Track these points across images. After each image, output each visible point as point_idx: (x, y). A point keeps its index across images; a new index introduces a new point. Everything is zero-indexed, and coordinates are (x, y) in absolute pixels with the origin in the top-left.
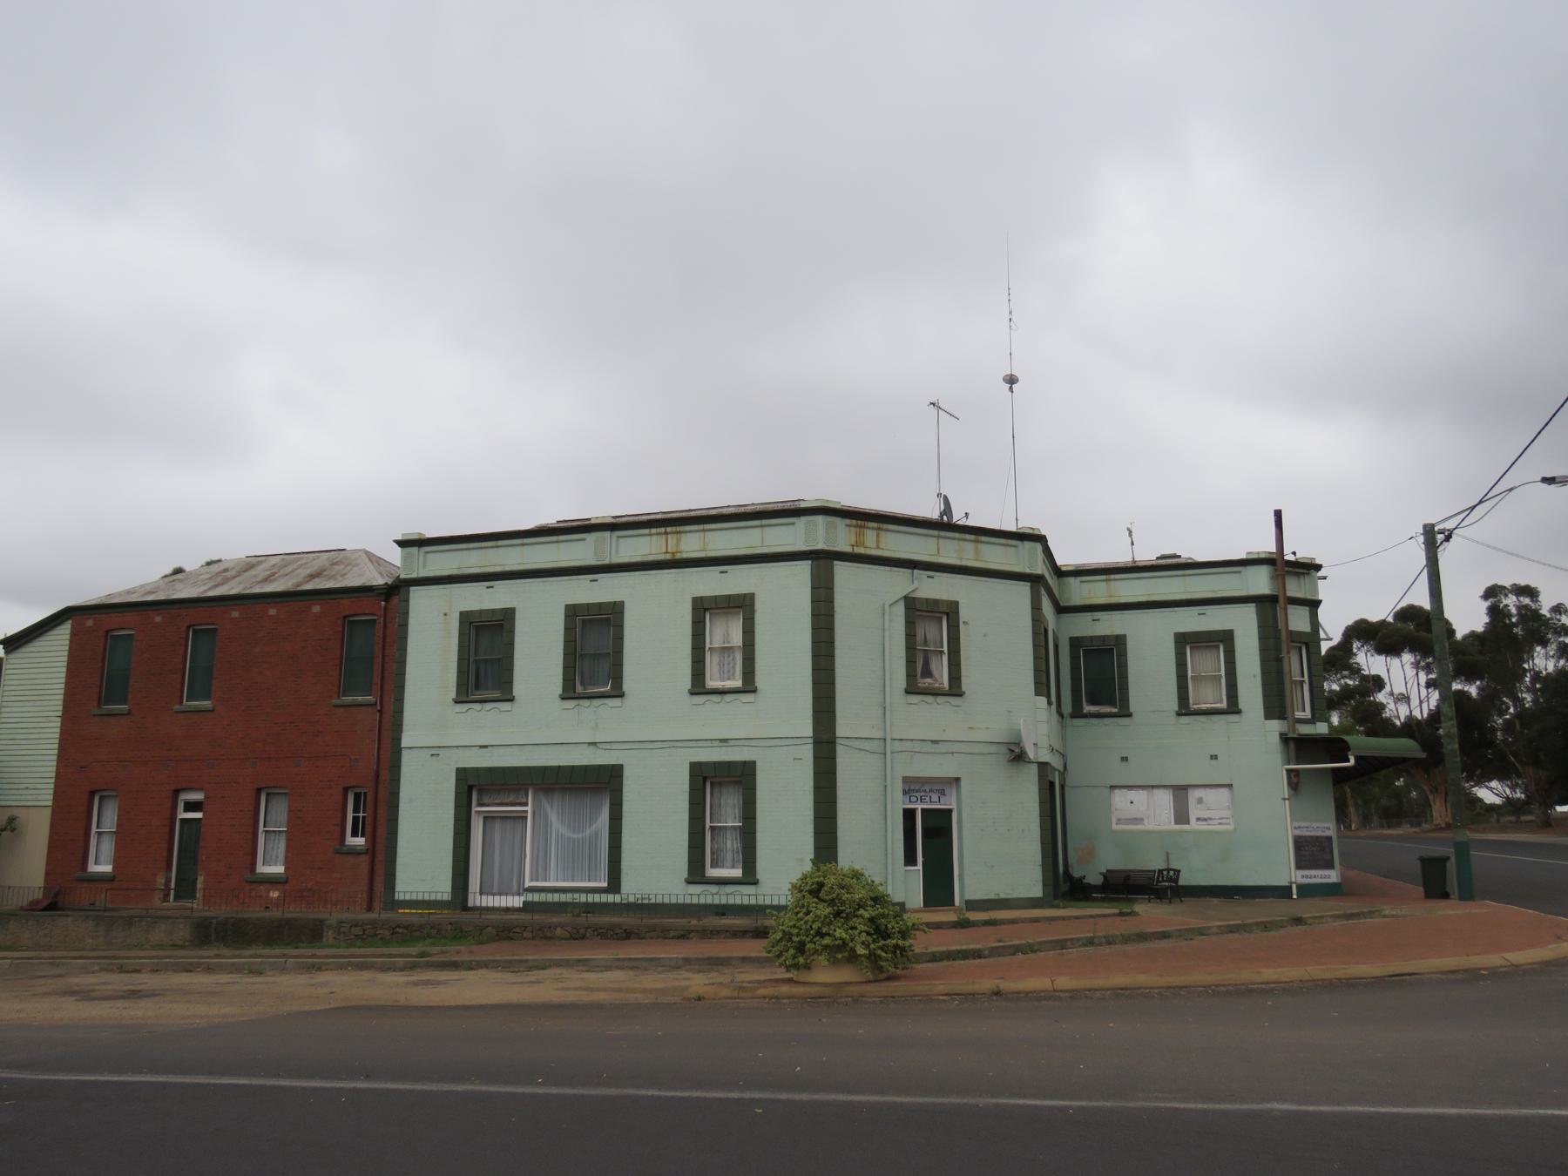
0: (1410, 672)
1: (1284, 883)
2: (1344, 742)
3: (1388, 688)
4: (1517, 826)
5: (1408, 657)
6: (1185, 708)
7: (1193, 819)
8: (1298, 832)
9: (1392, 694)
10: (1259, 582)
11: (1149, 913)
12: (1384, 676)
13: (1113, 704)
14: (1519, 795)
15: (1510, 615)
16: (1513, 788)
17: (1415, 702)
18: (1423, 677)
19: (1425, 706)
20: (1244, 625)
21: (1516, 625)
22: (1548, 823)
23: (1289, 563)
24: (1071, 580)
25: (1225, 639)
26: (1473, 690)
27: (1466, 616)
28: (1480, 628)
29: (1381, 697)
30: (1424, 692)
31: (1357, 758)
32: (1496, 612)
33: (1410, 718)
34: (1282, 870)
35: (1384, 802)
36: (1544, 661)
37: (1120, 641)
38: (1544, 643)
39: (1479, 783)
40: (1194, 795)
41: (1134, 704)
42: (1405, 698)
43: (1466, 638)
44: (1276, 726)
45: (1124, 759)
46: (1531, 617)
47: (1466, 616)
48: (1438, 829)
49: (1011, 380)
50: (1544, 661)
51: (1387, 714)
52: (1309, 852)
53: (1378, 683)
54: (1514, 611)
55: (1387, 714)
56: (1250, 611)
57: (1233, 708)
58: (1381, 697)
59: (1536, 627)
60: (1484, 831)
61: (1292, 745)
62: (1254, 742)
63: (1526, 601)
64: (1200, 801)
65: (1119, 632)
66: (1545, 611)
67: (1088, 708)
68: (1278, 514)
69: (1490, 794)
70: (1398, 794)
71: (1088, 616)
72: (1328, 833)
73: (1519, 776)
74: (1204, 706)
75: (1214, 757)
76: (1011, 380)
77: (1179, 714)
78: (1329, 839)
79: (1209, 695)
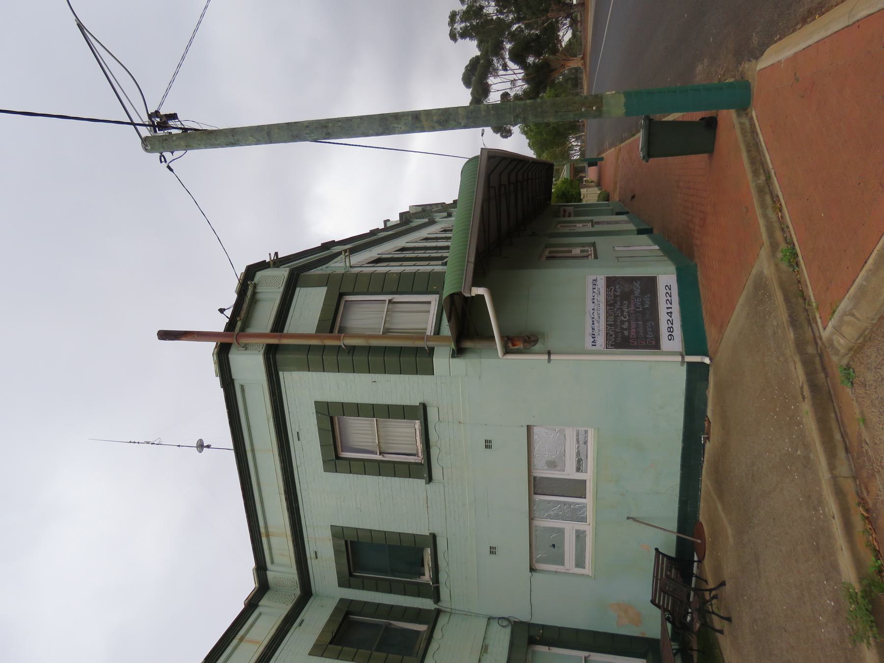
0: (498, 80)
1: (682, 374)
2: (452, 296)
3: (508, 91)
4: (584, 22)
5: (491, 80)
6: (423, 470)
7: (579, 476)
8: (601, 340)
9: (511, 88)
10: (249, 366)
11: (720, 563)
12: (501, 92)
13: (421, 551)
14: (568, 21)
15: (466, 26)
16: (565, 24)
17: (514, 77)
18: (501, 72)
19: (516, 72)
20: (306, 389)
21: (470, 23)
22: (582, 4)
23: (230, 326)
24: (270, 575)
25: (331, 416)
26: (508, 46)
27: (471, 49)
28: (475, 43)
29: (512, 94)
30: (510, 72)
31: (476, 284)
32: (465, 34)
33: (523, 79)
34: (659, 376)
35: (569, 86)
36: (491, 9)
37: (338, 533)
38: (481, 8)
39: (560, 42)
40: (543, 472)
41: (421, 528)
42: (513, 82)
43: (480, 50)
44: (442, 360)
45: (493, 551)
46: (467, 16)
47: (471, 49)
48: (584, 64)
49: (201, 446)
50: (491, 9)
51: (520, 93)
52: (630, 323)
53: (505, 96)
54: (463, 25)
55: (520, 93)
56: (291, 380)
57: (420, 412)
58: (512, 94)
59: (474, 12)
60: (586, 38)
61: (468, 344)
62: (466, 390)
63: (458, 17)
64: (552, 465)
65: (328, 534)
66: (465, 7)
67: (427, 577)
68: (164, 335)
69: (566, 36)
70: (566, 80)
71: (312, 564)
72: (602, 284)
73: (557, 22)
74: (420, 446)
75: (488, 445)
76: (201, 446)
77: (430, 479)
78: (611, 282)
79: (404, 436)
